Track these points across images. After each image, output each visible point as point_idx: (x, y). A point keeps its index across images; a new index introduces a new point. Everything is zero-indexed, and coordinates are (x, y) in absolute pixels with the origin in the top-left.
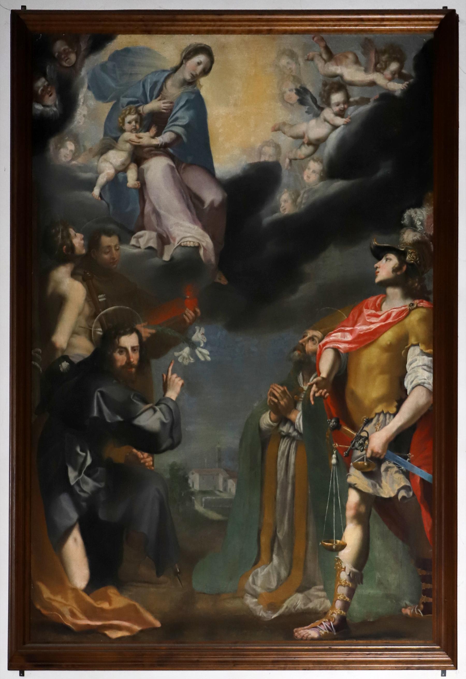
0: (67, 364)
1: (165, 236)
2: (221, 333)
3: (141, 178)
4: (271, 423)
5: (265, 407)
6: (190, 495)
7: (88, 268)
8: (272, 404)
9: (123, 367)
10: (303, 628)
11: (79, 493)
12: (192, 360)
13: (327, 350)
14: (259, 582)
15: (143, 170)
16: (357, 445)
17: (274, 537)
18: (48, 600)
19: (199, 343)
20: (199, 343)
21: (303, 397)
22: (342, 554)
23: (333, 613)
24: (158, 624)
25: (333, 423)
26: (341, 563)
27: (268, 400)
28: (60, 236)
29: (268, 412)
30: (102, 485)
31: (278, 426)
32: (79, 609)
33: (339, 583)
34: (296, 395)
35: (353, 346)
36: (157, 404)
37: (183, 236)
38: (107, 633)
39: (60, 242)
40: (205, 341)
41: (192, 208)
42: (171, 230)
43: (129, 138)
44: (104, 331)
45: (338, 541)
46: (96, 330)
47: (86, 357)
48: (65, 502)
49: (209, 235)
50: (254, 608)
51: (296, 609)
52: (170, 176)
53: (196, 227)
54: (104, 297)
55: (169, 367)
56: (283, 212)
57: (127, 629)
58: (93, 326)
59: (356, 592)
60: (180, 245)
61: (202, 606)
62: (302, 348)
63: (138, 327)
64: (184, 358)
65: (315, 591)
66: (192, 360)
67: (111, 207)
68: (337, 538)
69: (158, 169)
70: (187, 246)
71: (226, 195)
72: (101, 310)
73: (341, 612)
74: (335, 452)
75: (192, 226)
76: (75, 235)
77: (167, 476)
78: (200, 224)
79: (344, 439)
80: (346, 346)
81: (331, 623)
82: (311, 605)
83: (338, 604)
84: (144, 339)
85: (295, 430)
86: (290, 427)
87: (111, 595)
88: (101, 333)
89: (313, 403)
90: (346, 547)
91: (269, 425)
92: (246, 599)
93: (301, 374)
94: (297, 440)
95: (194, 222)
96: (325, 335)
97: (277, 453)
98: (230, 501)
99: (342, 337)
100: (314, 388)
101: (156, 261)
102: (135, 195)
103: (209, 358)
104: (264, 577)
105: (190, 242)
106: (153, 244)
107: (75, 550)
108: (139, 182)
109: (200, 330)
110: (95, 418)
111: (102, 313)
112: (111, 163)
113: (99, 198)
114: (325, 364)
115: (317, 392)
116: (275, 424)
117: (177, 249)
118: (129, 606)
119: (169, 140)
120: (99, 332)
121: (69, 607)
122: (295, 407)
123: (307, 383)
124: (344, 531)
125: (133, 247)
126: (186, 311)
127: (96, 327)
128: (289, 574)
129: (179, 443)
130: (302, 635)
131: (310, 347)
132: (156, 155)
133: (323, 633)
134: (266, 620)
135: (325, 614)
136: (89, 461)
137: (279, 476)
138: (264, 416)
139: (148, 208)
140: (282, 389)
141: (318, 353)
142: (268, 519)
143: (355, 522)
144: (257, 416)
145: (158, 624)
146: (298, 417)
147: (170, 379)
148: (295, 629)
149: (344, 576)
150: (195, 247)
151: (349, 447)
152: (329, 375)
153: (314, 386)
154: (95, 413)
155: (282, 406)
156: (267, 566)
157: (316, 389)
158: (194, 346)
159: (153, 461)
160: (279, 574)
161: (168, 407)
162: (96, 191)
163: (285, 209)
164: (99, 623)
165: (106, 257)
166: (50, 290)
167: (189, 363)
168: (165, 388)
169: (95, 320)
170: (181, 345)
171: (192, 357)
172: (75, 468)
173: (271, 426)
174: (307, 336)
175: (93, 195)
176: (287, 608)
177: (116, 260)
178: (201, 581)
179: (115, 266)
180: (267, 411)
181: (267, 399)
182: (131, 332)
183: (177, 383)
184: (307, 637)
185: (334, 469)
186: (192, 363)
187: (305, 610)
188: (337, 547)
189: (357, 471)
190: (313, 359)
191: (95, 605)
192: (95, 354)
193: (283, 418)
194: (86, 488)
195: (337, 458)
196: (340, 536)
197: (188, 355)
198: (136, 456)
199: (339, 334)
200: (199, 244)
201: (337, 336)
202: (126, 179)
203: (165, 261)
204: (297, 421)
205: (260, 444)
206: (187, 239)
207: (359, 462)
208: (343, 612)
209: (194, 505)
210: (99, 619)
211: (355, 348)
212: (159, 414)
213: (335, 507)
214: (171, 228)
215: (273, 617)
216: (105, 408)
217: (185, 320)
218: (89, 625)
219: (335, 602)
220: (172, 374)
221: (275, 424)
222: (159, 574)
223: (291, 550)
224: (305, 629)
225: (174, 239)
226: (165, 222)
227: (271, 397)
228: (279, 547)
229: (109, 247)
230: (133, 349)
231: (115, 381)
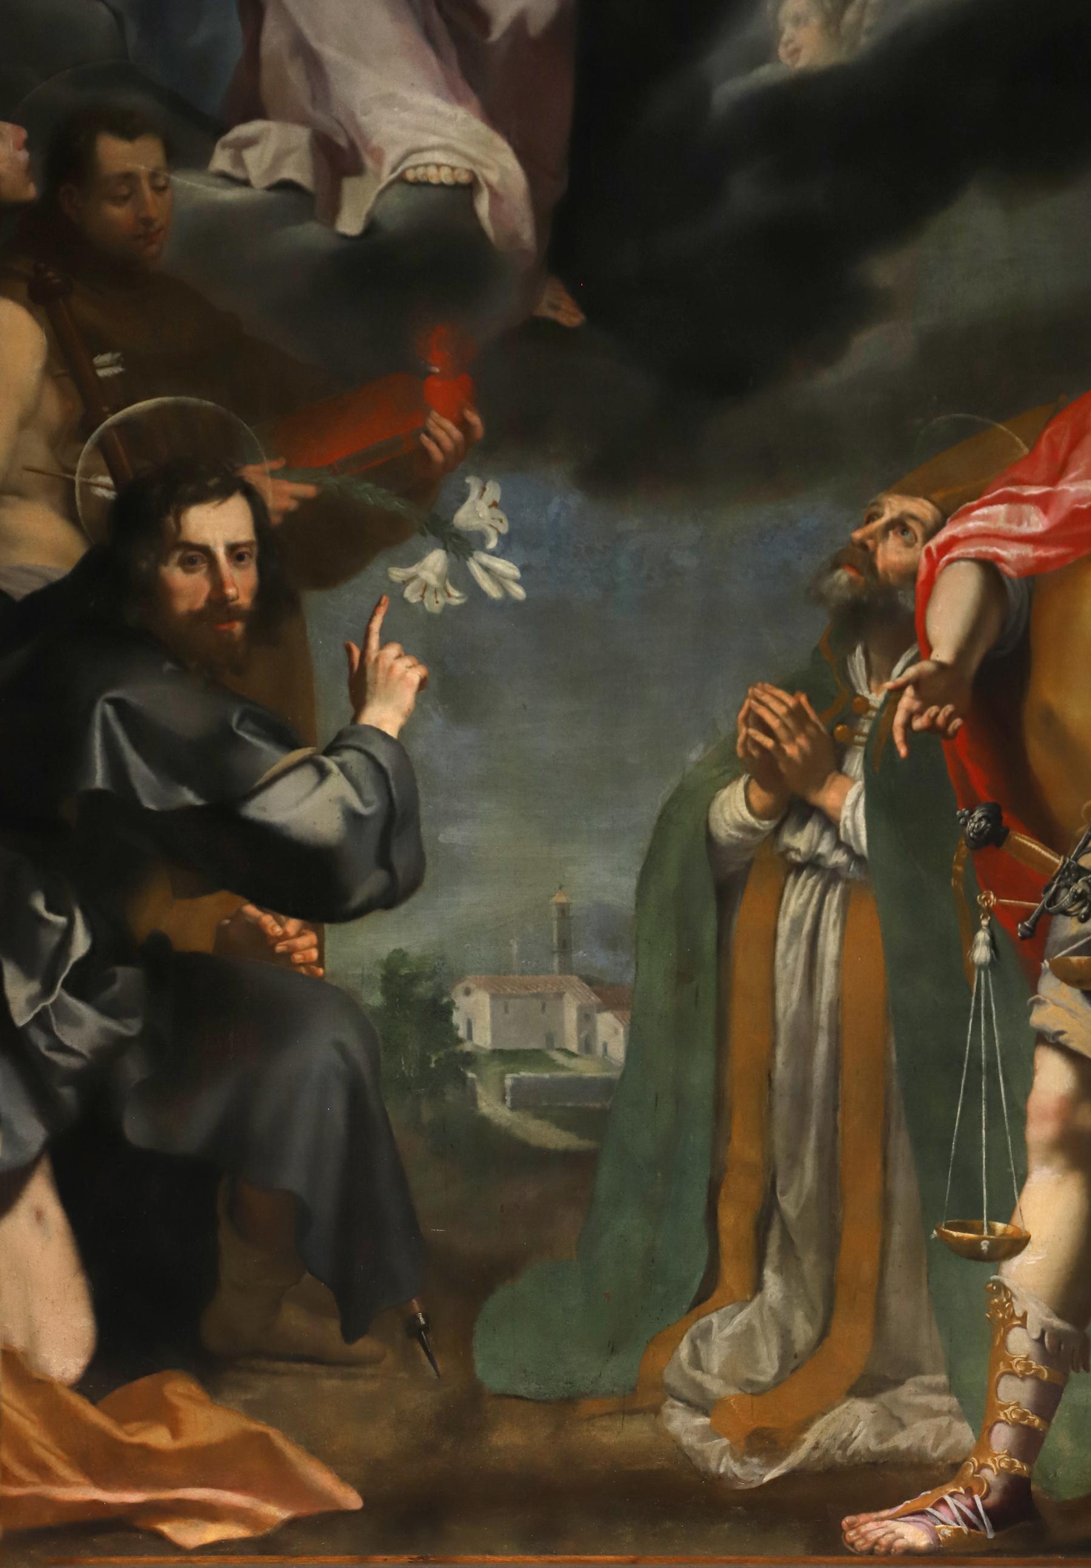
1: (342, 142)
2: (562, 502)
4: (751, 819)
8: (755, 753)
9: (197, 617)
10: (874, 1515)
11: (47, 1053)
12: (456, 597)
13: (955, 565)
14: (716, 1356)
16: (1065, 898)
17: (766, 1213)
19: (480, 539)
20: (480, 539)
21: (866, 729)
22: (1014, 1269)
23: (982, 1466)
24: (353, 1501)
25: (976, 822)
26: (1009, 1300)
27: (740, 739)
29: (741, 784)
30: (131, 1028)
31: (777, 831)
33: (1002, 1368)
34: (839, 724)
35: (1052, 553)
36: (331, 750)
37: (409, 145)
38: (166, 1528)
40: (504, 529)
41: (444, 37)
42: (364, 120)
44: (118, 484)
45: (1000, 1226)
47: (57, 577)
49: (511, 143)
50: (698, 1446)
51: (849, 1452)
55: (371, 620)
56: (788, 62)
58: (80, 465)
59: (1065, 1397)
60: (401, 179)
61: (511, 1440)
62: (862, 557)
64: (426, 587)
65: (916, 1394)
66: (456, 597)
68: (994, 1217)
70: (427, 184)
73: (1012, 1464)
74: (984, 922)
75: (445, 107)
77: (375, 999)
78: (475, 101)
79: (1019, 880)
80: (1028, 551)
81: (977, 1498)
82: (902, 1441)
83: (1002, 1437)
84: (276, 520)
85: (839, 844)
86: (821, 837)
87: (175, 1400)
89: (903, 751)
90: (1029, 1247)
91: (744, 828)
92: (670, 1419)
93: (859, 650)
94: (847, 881)
96: (946, 513)
98: (607, 1087)
99: (1009, 520)
100: (908, 701)
101: (309, 233)
103: (518, 592)
104: (732, 1343)
105: (440, 166)
106: (297, 170)
109: (484, 489)
110: (99, 792)
111: (111, 420)
114: (950, 616)
115: (920, 713)
116: (766, 823)
118: (248, 1439)
120: (104, 487)
122: (838, 766)
123: (880, 682)
124: (1020, 1191)
125: (219, 181)
126: (430, 423)
127: (88, 472)
128: (824, 1333)
130: (872, 1537)
131: (892, 554)
133: (948, 1532)
134: (741, 1486)
135: (952, 1469)
136: (81, 944)
137: (781, 1004)
138: (725, 793)
139: (273, 38)
140: (791, 702)
141: (922, 576)
142: (742, 1147)
143: (1059, 1161)
145: (353, 1501)
146: (848, 800)
147: (377, 660)
148: (848, 1520)
149: (1020, 1343)
150: (457, 186)
151: (1039, 906)
152: (963, 653)
153: (909, 691)
154: (99, 779)
155: (790, 761)
156: (744, 1303)
157: (916, 705)
158: (461, 545)
161: (371, 757)
163: (797, 51)
165: (118, 213)
168: (359, 690)
169: (88, 446)
170: (415, 541)
171: (455, 585)
172: (29, 972)
173: (753, 831)
174: (879, 516)
176: (816, 1447)
177: (157, 225)
178: (503, 1356)
179: (153, 249)
180: (736, 777)
181: (736, 735)
182: (223, 493)
183: (403, 677)
184: (890, 1546)
185: (981, 981)
187: (881, 1454)
188: (995, 1245)
189: (1066, 989)
190: (906, 601)
191: (120, 1434)
192: (88, 570)
193: (794, 805)
194: (70, 1037)
195: (993, 945)
196: (1006, 1209)
198: (257, 929)
199: (1001, 509)
201: (992, 516)
203: (344, 237)
204: (846, 813)
205: (708, 897)
206: (428, 157)
207: (1074, 959)
208: (1018, 1464)
209: (473, 1099)
210: (137, 1485)
211: (1061, 558)
212: (337, 785)
213: (987, 1108)
215: (766, 1479)
217: (425, 453)
218: (96, 1503)
219: (991, 1430)
220: (383, 644)
221: (766, 825)
222: (350, 1334)
223: (831, 1248)
224: (883, 1519)
225: (378, 155)
226: (340, 89)
227: (752, 731)
228: (787, 1244)
229: (129, 177)
230: (235, 552)
231: (168, 666)
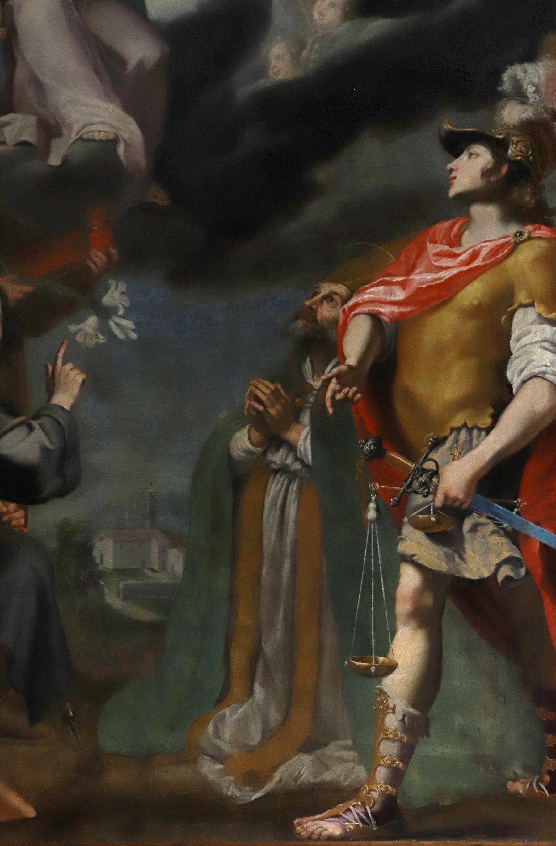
1: (52, 122)
4: (251, 447)
5: (240, 420)
6: (94, 577)
8: (254, 413)
14: (227, 734)
17: (256, 654)
24: (30, 812)
36: (34, 418)
40: (127, 304)
42: (63, 111)
49: (135, 120)
50: (218, 781)
53: (111, 106)
60: (81, 139)
61: (116, 778)
70: (94, 140)
75: (102, 104)
91: (248, 452)
95: (108, 98)
97: (264, 500)
103: (134, 336)
105: (100, 131)
109: (117, 286)
116: (259, 449)
134: (240, 802)
137: (265, 543)
138: (238, 434)
139: (20, 74)
142: (244, 618)
144: (223, 437)
145: (30, 812)
147: (61, 371)
150: (108, 141)
155: (271, 417)
158: (105, 313)
159: (26, 517)
161: (55, 420)
168: (51, 386)
171: (102, 334)
173: (252, 453)
180: (244, 426)
181: (243, 404)
200: (115, 134)
203: (52, 167)
209: (102, 595)
212: (38, 435)
217: (88, 267)
220: (64, 363)
225: (70, 128)
227: (252, 402)
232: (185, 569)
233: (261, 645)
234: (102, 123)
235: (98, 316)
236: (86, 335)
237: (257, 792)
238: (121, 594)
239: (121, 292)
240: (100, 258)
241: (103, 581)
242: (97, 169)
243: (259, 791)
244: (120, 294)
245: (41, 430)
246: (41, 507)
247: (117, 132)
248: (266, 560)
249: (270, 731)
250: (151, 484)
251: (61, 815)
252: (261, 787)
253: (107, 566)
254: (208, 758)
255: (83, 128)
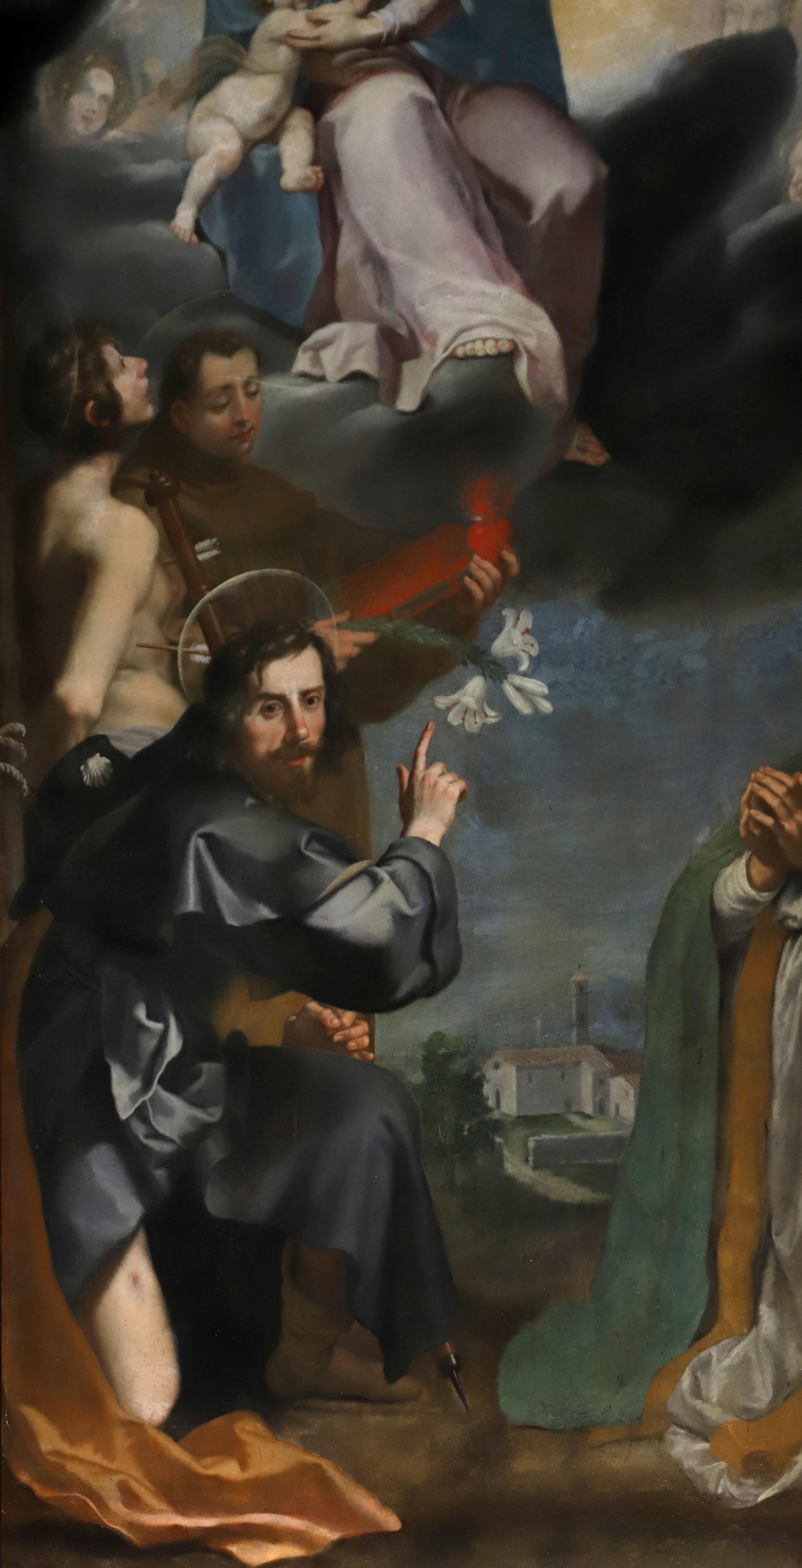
0: (105, 760)
1: (403, 331)
2: (585, 621)
3: (326, 157)
4: (752, 893)
5: (732, 845)
6: (488, 1130)
7: (164, 464)
8: (756, 832)
9: (274, 756)
11: (145, 1141)
14: (714, 1388)
15: (331, 127)
17: (762, 1254)
18: (53, 1459)
19: (515, 661)
20: (515, 661)
24: (392, 1522)
27: (743, 821)
28: (74, 373)
29: (743, 861)
30: (213, 1115)
32: (148, 1484)
36: (381, 863)
38: (234, 1549)
39: (75, 391)
40: (534, 652)
42: (421, 309)
43: (283, 31)
44: (212, 652)
46: (192, 649)
47: (161, 734)
48: (103, 1169)
49: (547, 310)
50: (699, 1469)
52: (419, 134)
53: (505, 291)
54: (214, 546)
55: (419, 744)
57: (295, 1537)
58: (182, 639)
60: (453, 357)
61: (531, 1467)
63: (321, 627)
67: (232, 261)
69: (379, 115)
70: (475, 357)
71: (604, 170)
72: (204, 587)
75: (490, 288)
76: (123, 365)
77: (417, 1077)
78: (516, 277)
84: (340, 666)
88: (205, 660)
91: (747, 901)
95: (501, 277)
97: (774, 984)
98: (618, 1144)
101: (375, 415)
102: (306, 212)
103: (546, 707)
105: (485, 341)
106: (365, 361)
107: (134, 1309)
108: (318, 169)
109: (518, 619)
111: (209, 595)
112: (230, 120)
113: (195, 238)
116: (766, 894)
117: (443, 371)
118: (304, 1469)
119: (415, 14)
120: (201, 654)
121: (116, 1478)
125: (300, 380)
126: (473, 565)
127: (188, 643)
129: (451, 974)
132: (372, 71)
134: (738, 1505)
136: (174, 1046)
137: (777, 1060)
138: (728, 870)
139: (348, 249)
142: (741, 1193)
144: (701, 875)
145: (392, 1522)
147: (423, 779)
150: (500, 355)
154: (191, 903)
155: (788, 836)
158: (497, 670)
159: (371, 1034)
160: (779, 1366)
161: (416, 864)
162: (185, 217)
164: (208, 1522)
165: (218, 420)
166: (48, 543)
167: (484, 725)
168: (408, 809)
169: (188, 621)
170: (458, 670)
171: (492, 706)
172: (131, 1072)
173: (753, 902)
175: (173, 231)
177: (249, 425)
179: (246, 445)
180: (739, 855)
181: (738, 817)
182: (298, 647)
183: (445, 792)
186: (494, 726)
194: (164, 1126)
197: (478, 701)
198: (319, 1023)
200: (513, 342)
202: (276, 166)
203: (403, 413)
209: (500, 1162)
210: (211, 1511)
212: (388, 891)
214: (423, 304)
215: (761, 1498)
216: (220, 884)
217: (467, 592)
218: (176, 1527)
220: (429, 764)
221: (766, 896)
222: (391, 1376)
225: (433, 339)
227: (753, 812)
229: (228, 388)
230: (307, 697)
231: (250, 801)
232: (638, 1111)
233: (772, 1238)
234: (493, 324)
235: (485, 677)
236: (466, 712)
237: (767, 1488)
238: (531, 1159)
239: (523, 630)
240: (487, 573)
241: (500, 1137)
242: (482, 413)
243: (771, 1486)
244: (523, 634)
245: (392, 883)
246: (399, 1013)
247: (517, 340)
248: (779, 1090)
249: (788, 1384)
250: (579, 967)
251: (442, 1528)
252: (774, 1480)
253: (507, 1112)
254: (682, 1431)
255: (455, 337)
